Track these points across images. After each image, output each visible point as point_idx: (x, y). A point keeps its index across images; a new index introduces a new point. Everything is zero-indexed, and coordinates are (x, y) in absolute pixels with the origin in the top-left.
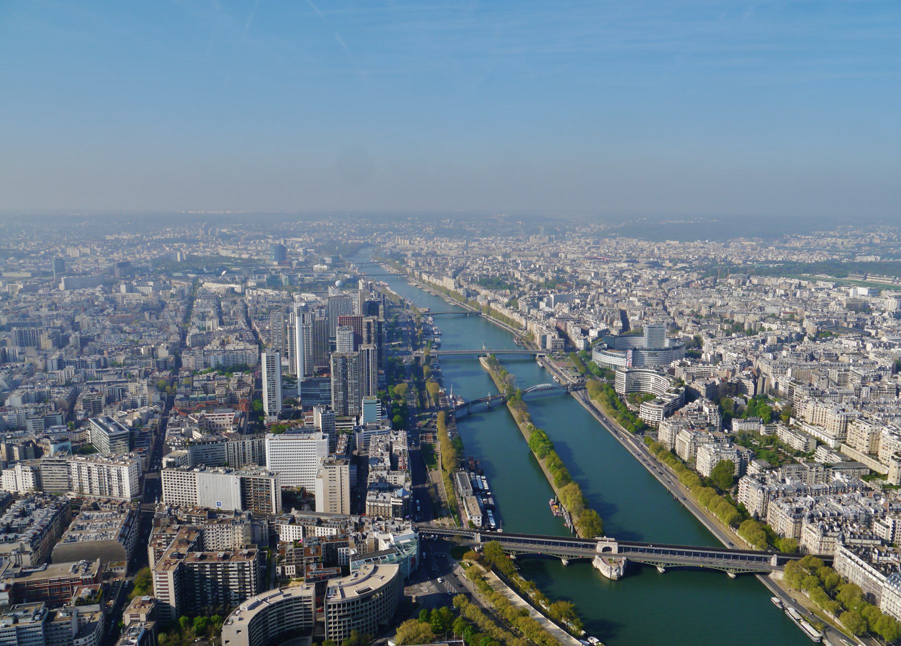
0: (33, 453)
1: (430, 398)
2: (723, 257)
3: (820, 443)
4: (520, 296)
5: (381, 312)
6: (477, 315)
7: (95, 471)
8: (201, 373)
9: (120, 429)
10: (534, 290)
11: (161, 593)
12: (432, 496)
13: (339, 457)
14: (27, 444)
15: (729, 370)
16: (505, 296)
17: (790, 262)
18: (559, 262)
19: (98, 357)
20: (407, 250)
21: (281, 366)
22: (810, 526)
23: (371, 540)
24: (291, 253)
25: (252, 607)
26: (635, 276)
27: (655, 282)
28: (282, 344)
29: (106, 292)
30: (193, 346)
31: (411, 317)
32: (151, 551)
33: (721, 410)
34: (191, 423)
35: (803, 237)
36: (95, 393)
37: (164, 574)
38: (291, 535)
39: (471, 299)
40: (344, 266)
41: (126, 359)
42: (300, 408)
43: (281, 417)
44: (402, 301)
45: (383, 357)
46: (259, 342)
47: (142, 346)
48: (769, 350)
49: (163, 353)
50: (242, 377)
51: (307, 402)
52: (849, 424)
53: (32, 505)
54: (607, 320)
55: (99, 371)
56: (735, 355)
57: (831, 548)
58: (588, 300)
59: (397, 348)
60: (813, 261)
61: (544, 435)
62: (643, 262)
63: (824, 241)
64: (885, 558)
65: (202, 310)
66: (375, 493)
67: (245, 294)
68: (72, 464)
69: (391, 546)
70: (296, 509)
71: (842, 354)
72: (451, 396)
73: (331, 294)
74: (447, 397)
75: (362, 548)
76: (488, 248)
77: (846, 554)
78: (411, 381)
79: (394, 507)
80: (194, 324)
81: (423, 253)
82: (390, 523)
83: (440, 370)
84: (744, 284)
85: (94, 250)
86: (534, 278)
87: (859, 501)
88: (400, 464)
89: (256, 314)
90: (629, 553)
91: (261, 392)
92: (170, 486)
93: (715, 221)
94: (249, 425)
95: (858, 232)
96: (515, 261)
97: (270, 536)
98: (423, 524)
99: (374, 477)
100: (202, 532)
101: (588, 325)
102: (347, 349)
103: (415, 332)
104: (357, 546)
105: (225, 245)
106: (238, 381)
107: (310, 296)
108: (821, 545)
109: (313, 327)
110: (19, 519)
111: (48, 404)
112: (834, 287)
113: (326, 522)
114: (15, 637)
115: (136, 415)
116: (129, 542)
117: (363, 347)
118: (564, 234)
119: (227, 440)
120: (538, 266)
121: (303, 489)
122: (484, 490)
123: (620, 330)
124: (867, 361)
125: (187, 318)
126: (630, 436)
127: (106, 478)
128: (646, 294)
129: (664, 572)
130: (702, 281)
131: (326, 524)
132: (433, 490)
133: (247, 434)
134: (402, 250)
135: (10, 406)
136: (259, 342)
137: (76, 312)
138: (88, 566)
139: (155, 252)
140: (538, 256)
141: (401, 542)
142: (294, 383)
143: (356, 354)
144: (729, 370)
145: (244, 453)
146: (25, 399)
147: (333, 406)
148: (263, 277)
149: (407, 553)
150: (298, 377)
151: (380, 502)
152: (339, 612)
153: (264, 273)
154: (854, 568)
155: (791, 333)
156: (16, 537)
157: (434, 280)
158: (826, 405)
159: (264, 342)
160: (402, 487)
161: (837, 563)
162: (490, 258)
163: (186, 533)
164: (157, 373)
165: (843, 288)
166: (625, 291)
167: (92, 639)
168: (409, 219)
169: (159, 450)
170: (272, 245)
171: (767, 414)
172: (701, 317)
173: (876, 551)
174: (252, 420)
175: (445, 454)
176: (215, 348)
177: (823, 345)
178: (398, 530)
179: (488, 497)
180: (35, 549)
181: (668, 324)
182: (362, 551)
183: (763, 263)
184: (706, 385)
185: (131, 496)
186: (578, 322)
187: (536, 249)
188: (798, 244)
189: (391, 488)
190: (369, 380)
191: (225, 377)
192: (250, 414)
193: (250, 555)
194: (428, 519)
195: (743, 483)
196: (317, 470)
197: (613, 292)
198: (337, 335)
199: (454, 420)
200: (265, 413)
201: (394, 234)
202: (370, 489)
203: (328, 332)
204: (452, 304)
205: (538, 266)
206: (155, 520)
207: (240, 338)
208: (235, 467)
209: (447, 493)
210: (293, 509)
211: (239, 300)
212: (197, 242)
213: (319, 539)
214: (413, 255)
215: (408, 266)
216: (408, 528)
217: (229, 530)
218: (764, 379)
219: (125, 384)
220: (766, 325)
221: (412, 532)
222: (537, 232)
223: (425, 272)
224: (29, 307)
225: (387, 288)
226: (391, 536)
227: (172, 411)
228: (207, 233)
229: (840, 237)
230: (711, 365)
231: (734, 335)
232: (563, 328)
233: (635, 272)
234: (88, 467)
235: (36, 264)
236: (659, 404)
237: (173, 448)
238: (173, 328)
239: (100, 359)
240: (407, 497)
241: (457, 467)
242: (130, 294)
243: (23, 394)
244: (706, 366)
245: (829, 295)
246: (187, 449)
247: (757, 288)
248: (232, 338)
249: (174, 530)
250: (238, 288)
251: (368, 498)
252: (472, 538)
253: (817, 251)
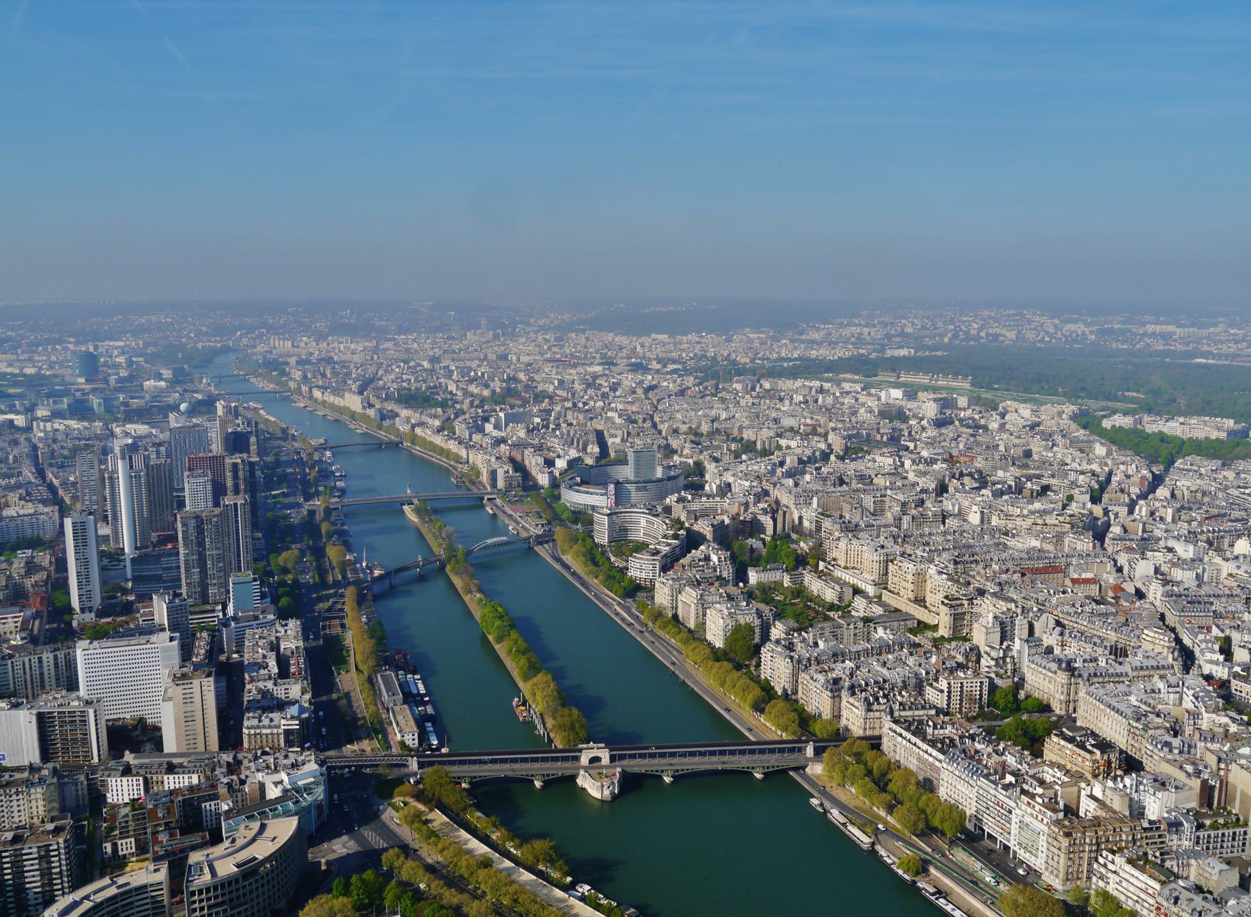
1: (333, 569)
4: (457, 416)
5: (253, 448)
10: (477, 407)
13: (197, 667)
16: (436, 417)
20: (289, 355)
22: (851, 700)
24: (105, 364)
26: (613, 383)
27: (640, 391)
31: (299, 453)
33: (733, 558)
39: (386, 423)
40: (192, 381)
42: (132, 598)
44: (284, 431)
45: (260, 513)
51: (142, 588)
52: (890, 564)
54: (578, 445)
56: (747, 484)
57: (877, 726)
58: (552, 418)
60: (836, 358)
63: (847, 332)
64: (941, 732)
66: (257, 715)
69: (285, 791)
70: (131, 752)
71: (876, 475)
72: (364, 564)
74: (358, 565)
75: (240, 798)
76: (408, 350)
77: (895, 732)
79: (287, 732)
81: (313, 359)
83: (346, 527)
88: (293, 669)
89: (53, 458)
90: (625, 762)
94: (47, 630)
96: (447, 367)
99: (254, 692)
103: (306, 475)
104: (232, 797)
106: (27, 563)
107: (141, 429)
113: (181, 766)
117: (228, 500)
120: (479, 374)
121: (141, 720)
124: (906, 482)
129: (764, 779)
131: (181, 770)
132: (344, 702)
133: (45, 644)
134: (281, 356)
140: (480, 360)
141: (300, 783)
142: (121, 561)
143: (217, 511)
145: (42, 674)
147: (184, 591)
148: (62, 402)
149: (309, 798)
150: (127, 550)
151: (264, 727)
154: (906, 748)
157: (331, 399)
158: (862, 542)
160: (297, 702)
161: (886, 745)
162: (412, 364)
166: (600, 404)
168: (289, 310)
170: (74, 353)
173: (931, 723)
175: (359, 649)
177: (853, 465)
178: (295, 766)
179: (425, 704)
183: (775, 361)
186: (539, 449)
187: (476, 350)
188: (816, 336)
191: (3, 558)
192: (49, 613)
198: (186, 485)
199: (370, 597)
200: (74, 609)
201: (268, 333)
202: (248, 709)
204: (360, 431)
205: (479, 374)
207: (27, 497)
210: (127, 752)
211: (22, 438)
213: (172, 792)
214: (298, 363)
215: (291, 379)
216: (309, 761)
217: (21, 796)
218: (785, 513)
221: (316, 767)
223: (317, 387)
225: (262, 412)
226: (283, 776)
230: (718, 499)
231: (744, 457)
232: (519, 458)
233: (613, 377)
241: (379, 665)
245: (857, 400)
248: (13, 497)
250: (20, 420)
251: (246, 723)
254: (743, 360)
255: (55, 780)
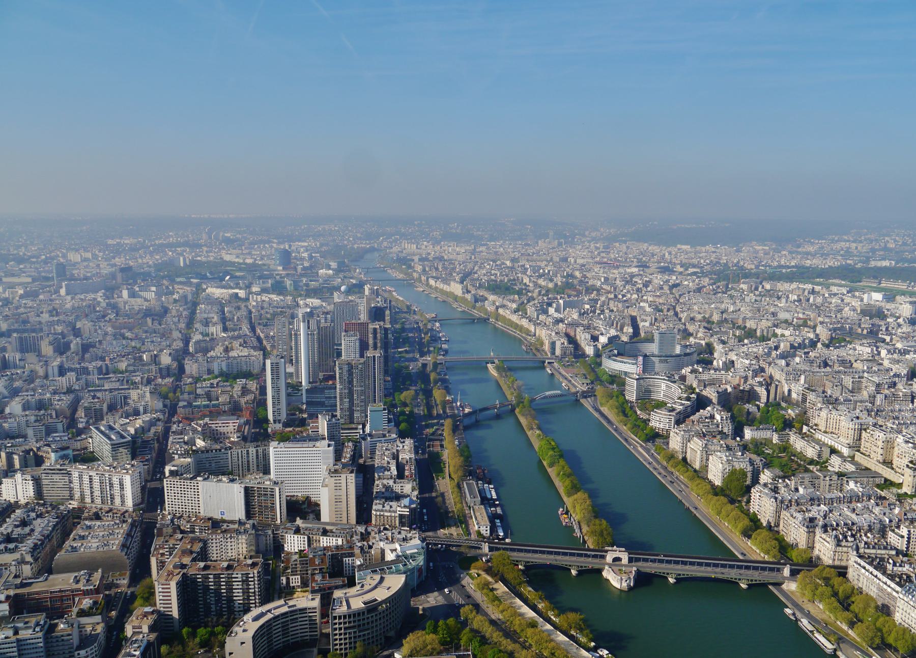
0: (33, 461)
1: (437, 405)
2: (735, 261)
3: (833, 451)
4: (529, 301)
5: (387, 318)
6: (485, 320)
7: (96, 479)
8: (205, 380)
9: (123, 437)
10: (543, 295)
11: (164, 604)
12: (439, 505)
13: (344, 466)
14: (27, 452)
15: (741, 377)
16: (514, 301)
17: (803, 267)
18: (568, 266)
19: (100, 363)
20: (414, 254)
21: (286, 373)
22: (824, 536)
23: (377, 550)
24: (296, 258)
25: (256, 619)
26: (646, 281)
27: (666, 288)
28: (286, 351)
29: (108, 298)
30: (196, 353)
31: (418, 323)
32: (153, 561)
33: (733, 418)
34: (195, 431)
35: (817, 241)
36: (96, 400)
37: (166, 585)
38: (296, 545)
39: (478, 304)
40: (349, 271)
41: (128, 365)
42: (305, 416)
43: (286, 425)
44: (408, 307)
45: (390, 364)
46: (263, 349)
47: (144, 352)
48: (782, 356)
49: (166, 360)
50: (246, 384)
51: (312, 410)
52: (863, 432)
53: (33, 515)
54: (617, 326)
55: (101, 378)
56: (747, 362)
57: (844, 558)
58: (598, 306)
59: (404, 355)
60: (827, 266)
61: (553, 443)
62: (653, 267)
63: (838, 246)
64: (900, 569)
65: (206, 316)
66: (381, 502)
67: (249, 299)
68: (73, 473)
69: (398, 556)
70: (301, 518)
71: (856, 361)
72: (458, 404)
73: (336, 300)
74: (454, 404)
75: (368, 558)
76: (496, 253)
77: (860, 565)
78: (418, 388)
79: (401, 516)
80: (197, 330)
81: (430, 258)
82: (396, 533)
83: (447, 377)
84: (756, 289)
85: (96, 255)
86: (543, 283)
87: (874, 511)
88: (407, 473)
89: (260, 320)
90: (640, 564)
91: (266, 400)
92: (173, 495)
93: (727, 225)
94: (253, 433)
95: (872, 237)
96: (523, 266)
97: (274, 546)
98: (430, 534)
99: (381, 486)
100: (205, 542)
101: (598, 331)
102: (353, 356)
103: (422, 339)
104: (363, 556)
105: (229, 250)
106: (242, 388)
107: (315, 302)
108: (835, 555)
109: (319, 333)
110: (19, 529)
111: (49, 412)
112: (848, 292)
113: (331, 531)
114: (15, 649)
115: (139, 423)
116: (131, 552)
117: (369, 353)
118: (573, 239)
119: (231, 448)
120: (546, 271)
121: (308, 498)
122: (492, 499)
123: (630, 336)
124: (881, 368)
125: (190, 324)
126: (640, 444)
127: (108, 487)
128: (657, 300)
129: (675, 583)
130: (714, 286)
131: (331, 534)
132: (440, 499)
133: (251, 442)
134: (409, 255)
135: (10, 414)
136: (263, 349)
137: (78, 318)
138: (90, 576)
139: (158, 257)
140: (547, 261)
141: (408, 552)
142: (299, 390)
143: (362, 360)
144: (741, 377)
145: (248, 461)
146: (26, 407)
147: (338, 413)
148: (268, 282)
149: (414, 563)
150: (303, 384)
151: (386, 511)
152: (345, 623)
153: (268, 278)
154: (868, 579)
155: (804, 339)
156: (16, 547)
157: (441, 286)
158: (840, 413)
159: (269, 348)
160: (408, 496)
161: (851, 574)
162: (498, 263)
163: (189, 542)
164: (160, 380)
165: (857, 294)
166: (635, 296)
167: (93, 651)
168: (416, 223)
169: (162, 458)
170: (276, 249)
171: (780, 421)
172: (713, 323)
173: (891, 561)
174: (257, 428)
175: (452, 463)
176: (219, 355)
177: (836, 352)
178: (405, 540)
179: (496, 506)
180: (36, 560)
181: (679, 330)
182: (368, 561)
183: (775, 268)
184: (718, 392)
185: (134, 506)
186: (588, 328)
187: (545, 254)
188: (811, 249)
189: (398, 497)
190: (375, 387)
191: (228, 384)
192: (254, 421)
193: (254, 565)
194: (435, 529)
195: (755, 492)
196: (322, 479)
197: (623, 297)
198: (343, 341)
199: (461, 427)
200: (269, 420)
201: (400, 238)
202: (376, 498)
203: (333, 338)
204: (460, 310)
205: (546, 271)
206: (158, 529)
207: (244, 344)
208: (239, 476)
209: (455, 502)
210: (298, 518)
211: (242, 305)
212: (200, 246)
213: (325, 549)
214: (420, 260)
215: (415, 271)
216: (415, 538)
217: (233, 540)
218: (777, 386)
219: (127, 391)
220: (779, 331)
221: (419, 542)
222: (546, 236)
223: (432, 277)
224: (29, 312)
225: (394, 293)
226: (397, 546)
227: (175, 419)
228: (210, 238)
229: (854, 242)
230: (723, 372)
231: (746, 341)
232: (572, 334)
233: (646, 277)
234: (90, 476)
235: (37, 269)
236: (670, 411)
237: (176, 457)
238: (176, 334)
239: (101, 366)
240: (413, 506)
241: (465, 476)
242: (132, 300)
243: (24, 401)
244: (718, 372)
245: (843, 300)
246: (191, 457)
247: (769, 293)
248: (236, 344)
249: (177, 540)
250: (242, 293)
251: (374, 507)
252: (480, 548)
253: (831, 256)
254: (749, 266)
255: (253, 532)
